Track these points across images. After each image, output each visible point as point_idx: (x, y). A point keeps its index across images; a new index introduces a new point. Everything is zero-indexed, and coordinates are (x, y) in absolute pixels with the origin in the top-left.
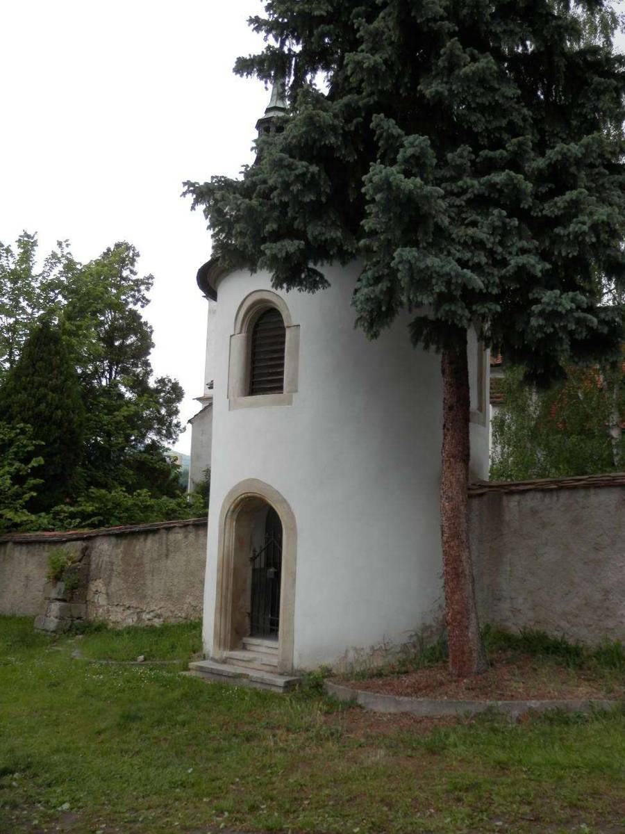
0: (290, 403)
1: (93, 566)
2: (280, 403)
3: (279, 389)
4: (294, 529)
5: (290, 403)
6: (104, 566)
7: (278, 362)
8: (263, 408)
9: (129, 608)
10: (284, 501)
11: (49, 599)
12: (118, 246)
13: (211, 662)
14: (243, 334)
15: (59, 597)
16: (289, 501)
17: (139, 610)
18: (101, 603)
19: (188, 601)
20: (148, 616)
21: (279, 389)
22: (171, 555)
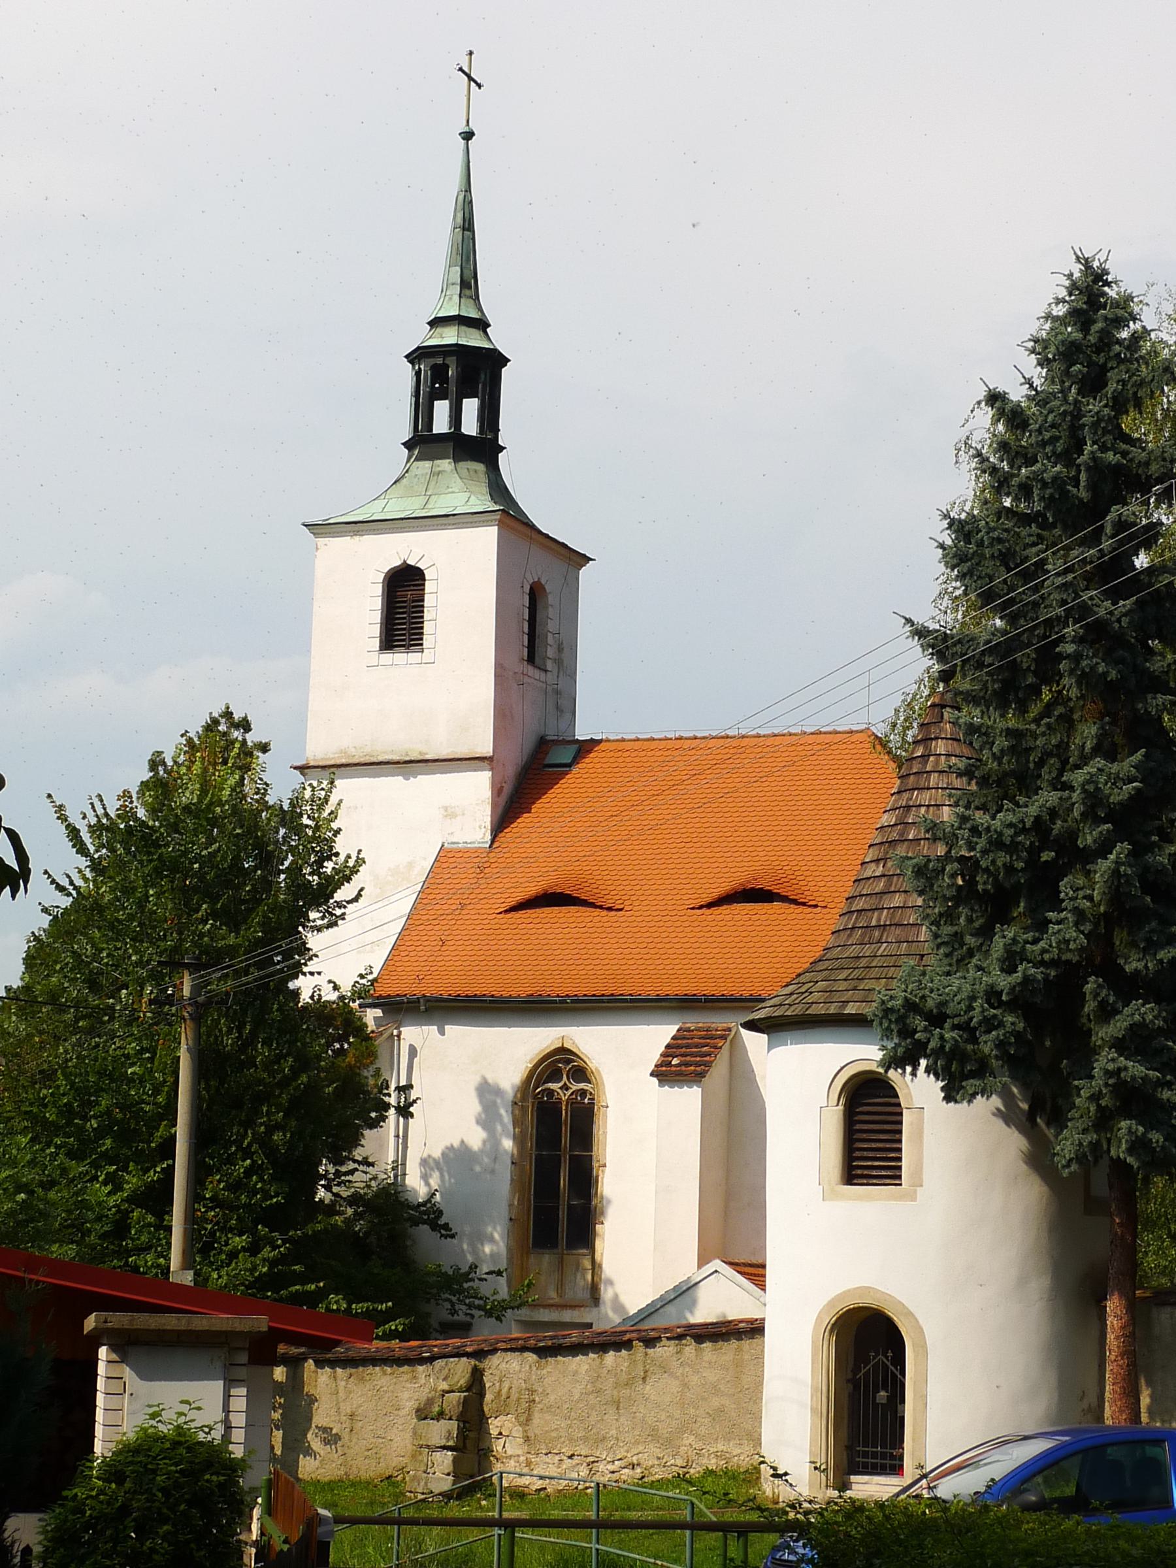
0: (913, 1198)
1: (489, 1397)
2: (902, 1198)
3: (893, 1176)
4: (922, 1347)
5: (913, 1198)
6: (514, 1396)
7: (895, 1146)
8: (870, 1203)
9: (571, 1457)
10: (910, 1314)
11: (428, 1447)
12: (211, 726)
13: (996, 1455)
14: (841, 1107)
15: (451, 1443)
16: (917, 1315)
17: (592, 1459)
18: (509, 1453)
19: (687, 1442)
20: (611, 1467)
21: (893, 1176)
22: (650, 1381)
